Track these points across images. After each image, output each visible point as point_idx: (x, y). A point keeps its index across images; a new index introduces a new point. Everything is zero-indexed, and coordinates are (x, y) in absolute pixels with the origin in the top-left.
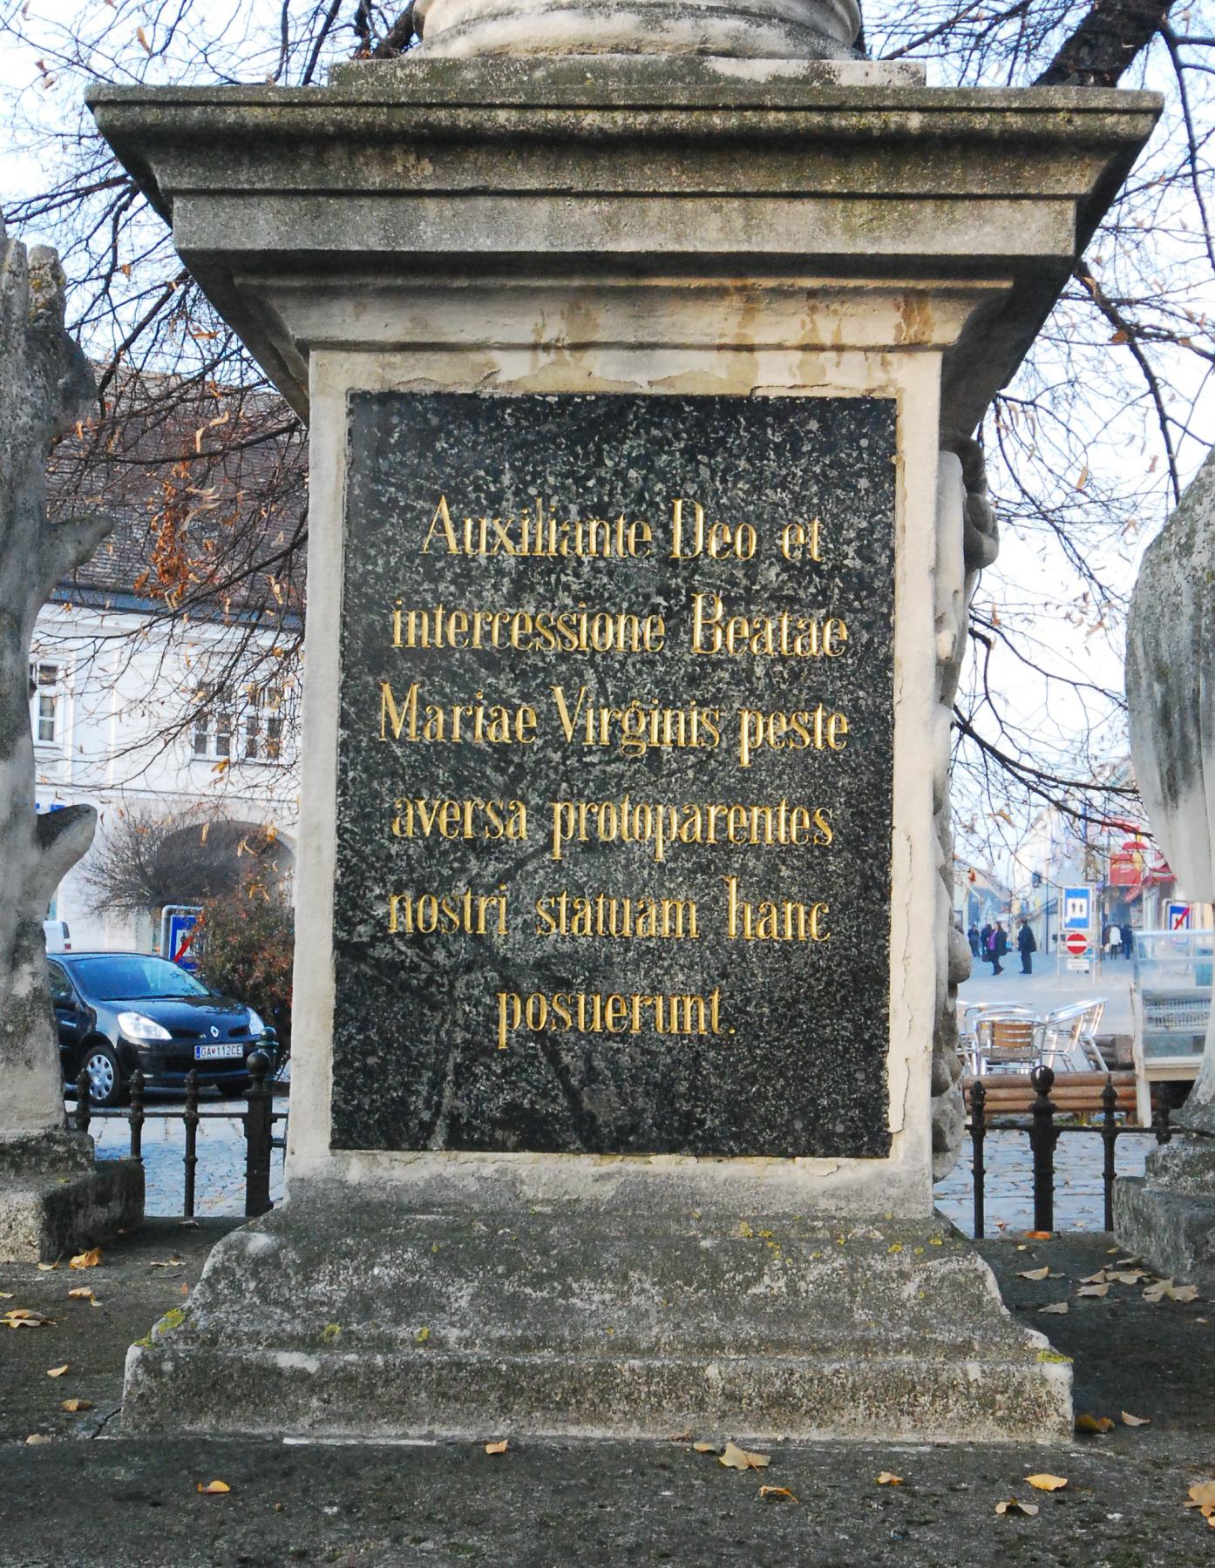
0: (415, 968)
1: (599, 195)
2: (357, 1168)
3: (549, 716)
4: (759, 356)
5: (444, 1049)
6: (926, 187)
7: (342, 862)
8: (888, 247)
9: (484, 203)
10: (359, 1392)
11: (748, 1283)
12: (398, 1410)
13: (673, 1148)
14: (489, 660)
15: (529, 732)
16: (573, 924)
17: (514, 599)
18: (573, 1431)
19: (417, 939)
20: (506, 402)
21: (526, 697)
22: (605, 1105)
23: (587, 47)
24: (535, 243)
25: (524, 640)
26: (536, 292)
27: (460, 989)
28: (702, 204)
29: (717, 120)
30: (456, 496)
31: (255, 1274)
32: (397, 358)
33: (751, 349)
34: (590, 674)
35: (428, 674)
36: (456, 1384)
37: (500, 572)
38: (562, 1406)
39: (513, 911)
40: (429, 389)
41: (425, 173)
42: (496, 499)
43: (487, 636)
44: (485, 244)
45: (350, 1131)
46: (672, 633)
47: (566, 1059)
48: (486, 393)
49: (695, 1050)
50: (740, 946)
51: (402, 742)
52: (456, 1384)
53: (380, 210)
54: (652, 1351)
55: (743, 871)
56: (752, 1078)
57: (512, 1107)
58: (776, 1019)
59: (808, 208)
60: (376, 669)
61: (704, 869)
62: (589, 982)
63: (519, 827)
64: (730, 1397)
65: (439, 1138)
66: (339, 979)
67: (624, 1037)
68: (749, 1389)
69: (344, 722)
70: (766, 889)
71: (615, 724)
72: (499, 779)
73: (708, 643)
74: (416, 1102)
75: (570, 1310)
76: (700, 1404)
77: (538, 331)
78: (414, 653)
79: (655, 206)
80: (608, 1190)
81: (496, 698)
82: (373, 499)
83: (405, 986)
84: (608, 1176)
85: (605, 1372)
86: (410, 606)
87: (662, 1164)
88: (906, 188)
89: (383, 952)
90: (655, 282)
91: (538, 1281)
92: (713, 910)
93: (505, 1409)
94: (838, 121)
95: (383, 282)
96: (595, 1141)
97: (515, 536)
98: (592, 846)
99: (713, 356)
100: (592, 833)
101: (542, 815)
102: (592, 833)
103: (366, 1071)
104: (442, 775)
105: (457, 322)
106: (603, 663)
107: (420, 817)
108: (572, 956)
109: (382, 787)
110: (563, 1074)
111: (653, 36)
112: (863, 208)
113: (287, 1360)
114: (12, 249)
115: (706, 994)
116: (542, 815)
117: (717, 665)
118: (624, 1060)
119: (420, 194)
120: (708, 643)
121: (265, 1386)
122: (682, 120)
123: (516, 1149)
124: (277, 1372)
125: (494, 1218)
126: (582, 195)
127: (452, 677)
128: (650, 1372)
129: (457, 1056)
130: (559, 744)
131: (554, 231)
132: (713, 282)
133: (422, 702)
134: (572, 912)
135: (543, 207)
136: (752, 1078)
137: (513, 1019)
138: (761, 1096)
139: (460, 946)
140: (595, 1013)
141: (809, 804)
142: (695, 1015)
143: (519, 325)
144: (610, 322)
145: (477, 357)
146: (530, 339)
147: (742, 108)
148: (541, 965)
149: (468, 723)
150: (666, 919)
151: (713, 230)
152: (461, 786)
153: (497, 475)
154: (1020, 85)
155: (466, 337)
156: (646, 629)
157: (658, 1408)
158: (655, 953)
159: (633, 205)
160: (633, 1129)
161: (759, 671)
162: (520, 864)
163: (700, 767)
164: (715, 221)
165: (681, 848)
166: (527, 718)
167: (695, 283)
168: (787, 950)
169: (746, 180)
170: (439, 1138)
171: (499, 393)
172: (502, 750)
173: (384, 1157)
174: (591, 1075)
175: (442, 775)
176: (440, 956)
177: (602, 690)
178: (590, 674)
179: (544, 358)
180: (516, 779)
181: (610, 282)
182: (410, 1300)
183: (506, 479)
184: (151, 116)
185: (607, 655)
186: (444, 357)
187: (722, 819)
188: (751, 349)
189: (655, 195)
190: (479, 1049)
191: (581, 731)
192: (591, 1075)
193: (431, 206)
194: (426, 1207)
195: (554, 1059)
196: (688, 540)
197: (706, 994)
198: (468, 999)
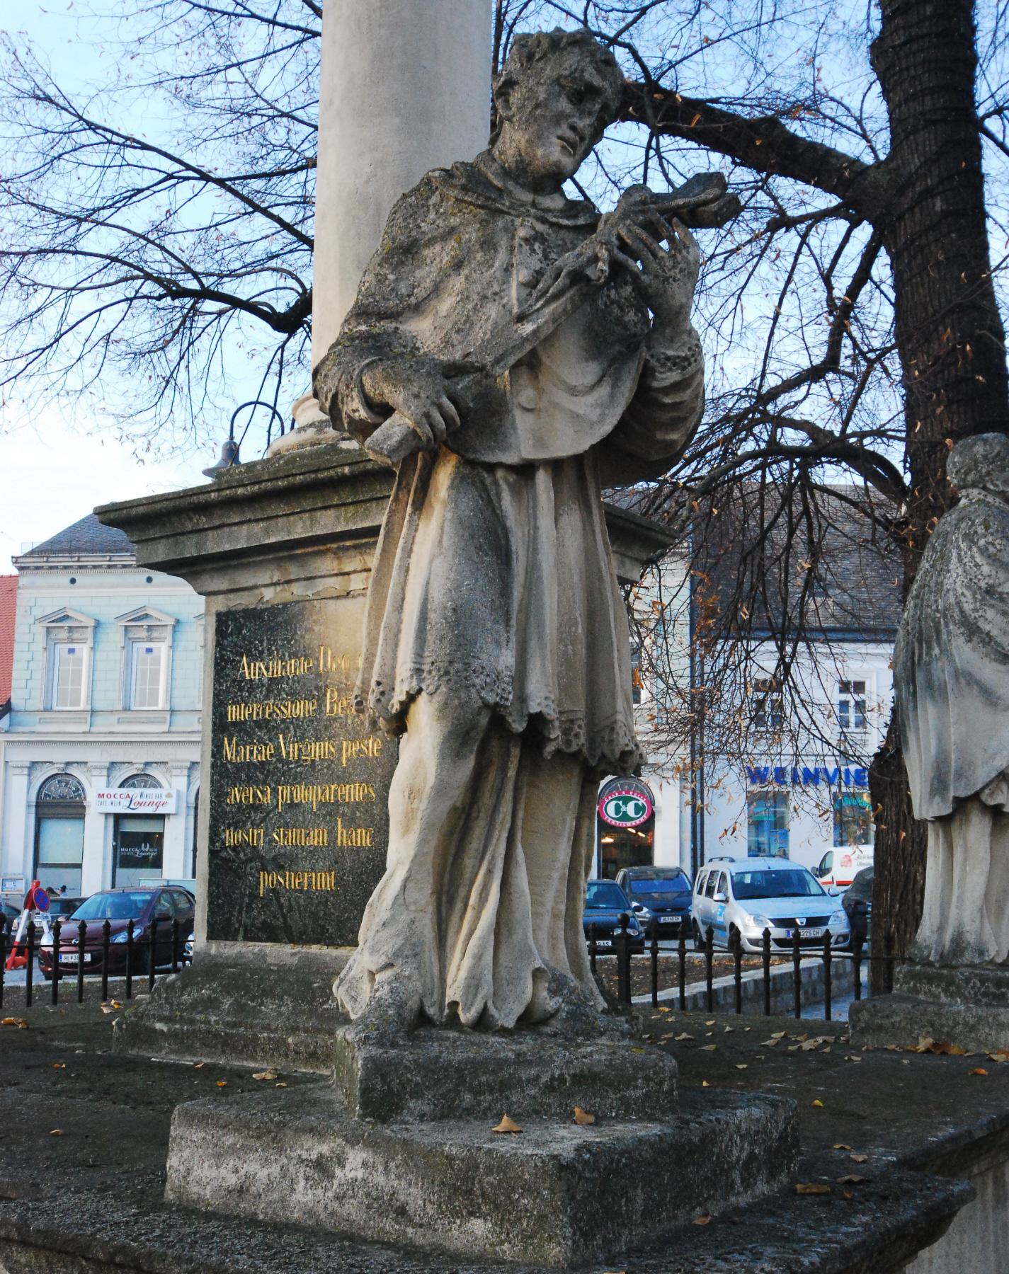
0: (234, 861)
1: (262, 520)
2: (214, 949)
3: (278, 748)
4: (352, 576)
5: (242, 896)
6: (368, 496)
7: (212, 816)
8: (360, 525)
9: (227, 529)
10: (181, 1041)
11: (324, 1003)
12: (190, 1050)
13: (318, 942)
14: (258, 724)
15: (271, 755)
16: (285, 839)
17: (267, 697)
18: (245, 1063)
19: (235, 849)
20: (265, 610)
21: (270, 740)
22: (296, 920)
23: (301, 446)
24: (242, 544)
25: (270, 715)
26: (261, 562)
27: (248, 870)
28: (296, 517)
29: (240, 491)
30: (249, 654)
31: (166, 991)
32: (231, 596)
33: (348, 574)
34: (292, 728)
35: (239, 732)
36: (212, 1041)
37: (263, 686)
38: (241, 1052)
39: (266, 835)
40: (241, 608)
41: (203, 522)
42: (261, 653)
43: (258, 714)
44: (227, 547)
45: (212, 935)
46: (320, 706)
47: (282, 900)
48: (260, 606)
49: (325, 896)
50: (342, 847)
51: (231, 763)
52: (212, 1041)
53: (194, 539)
54: (276, 1030)
55: (343, 814)
56: (345, 910)
57: (264, 922)
58: (355, 882)
59: (331, 513)
60: (223, 732)
61: (329, 814)
62: (290, 866)
63: (267, 800)
64: (297, 1053)
65: (240, 937)
66: (210, 866)
67: (301, 891)
68: (302, 1049)
69: (213, 756)
70: (351, 823)
71: (300, 750)
72: (261, 777)
73: (332, 711)
74: (234, 919)
75: (260, 1011)
76: (287, 1055)
77: (272, 578)
78: (234, 724)
79: (281, 520)
80: (295, 960)
81: (261, 741)
82: (222, 656)
83: (230, 868)
84: (295, 954)
85: (255, 1038)
86: (234, 703)
87: (315, 949)
88: (362, 498)
89: (224, 854)
90: (298, 552)
91: (253, 999)
92: (332, 833)
93: (224, 1052)
94: (320, 476)
95: (210, 566)
96: (293, 940)
97: (267, 669)
98: (292, 806)
99: (334, 579)
100: (292, 799)
101: (275, 791)
102: (292, 799)
103: (218, 905)
104: (243, 776)
105: (245, 578)
106: (296, 722)
107: (237, 795)
108: (284, 855)
109: (224, 782)
110: (281, 907)
111: (321, 437)
112: (351, 509)
113: (159, 1026)
114: (372, 540)
115: (330, 871)
116: (275, 791)
117: (335, 719)
118: (302, 901)
119: (206, 530)
120: (332, 711)
121: (151, 1038)
122: (269, 485)
123: (266, 941)
124: (155, 1030)
125: (254, 971)
126: (257, 521)
127: (247, 733)
128: (270, 1039)
129: (247, 900)
130: (280, 760)
131: (249, 538)
132: (316, 548)
133: (237, 745)
134: (285, 835)
135: (245, 527)
136: (345, 910)
137: (267, 881)
138: (349, 918)
139: (248, 851)
140: (290, 881)
141: (367, 782)
142: (325, 881)
143: (263, 576)
144: (294, 571)
145: (257, 592)
146: (269, 582)
147: (287, 476)
148: (274, 859)
149: (251, 752)
150: (317, 838)
151: (300, 529)
152: (250, 781)
153: (261, 642)
154: (773, 384)
155: (250, 584)
156: (311, 707)
157: (273, 1055)
158: (313, 852)
159: (273, 522)
160: (305, 933)
161: (350, 722)
162: (268, 814)
163: (329, 767)
164: (300, 524)
165: (322, 805)
166: (271, 749)
167: (310, 550)
168: (358, 850)
169: (307, 505)
170: (240, 937)
171: (263, 607)
172: (262, 763)
173: (223, 943)
174: (291, 908)
175: (243, 776)
176: (242, 855)
177: (295, 736)
178: (292, 728)
179: (279, 588)
180: (267, 776)
181: (281, 554)
182: (210, 1004)
183: (265, 644)
184: (158, 506)
185: (298, 719)
186: (246, 593)
187: (336, 791)
188: (348, 574)
189: (278, 516)
190: (254, 896)
191: (288, 753)
192: (291, 908)
193: (210, 533)
194: (234, 966)
195: (278, 900)
196: (325, 665)
197: (330, 871)
198: (251, 874)
